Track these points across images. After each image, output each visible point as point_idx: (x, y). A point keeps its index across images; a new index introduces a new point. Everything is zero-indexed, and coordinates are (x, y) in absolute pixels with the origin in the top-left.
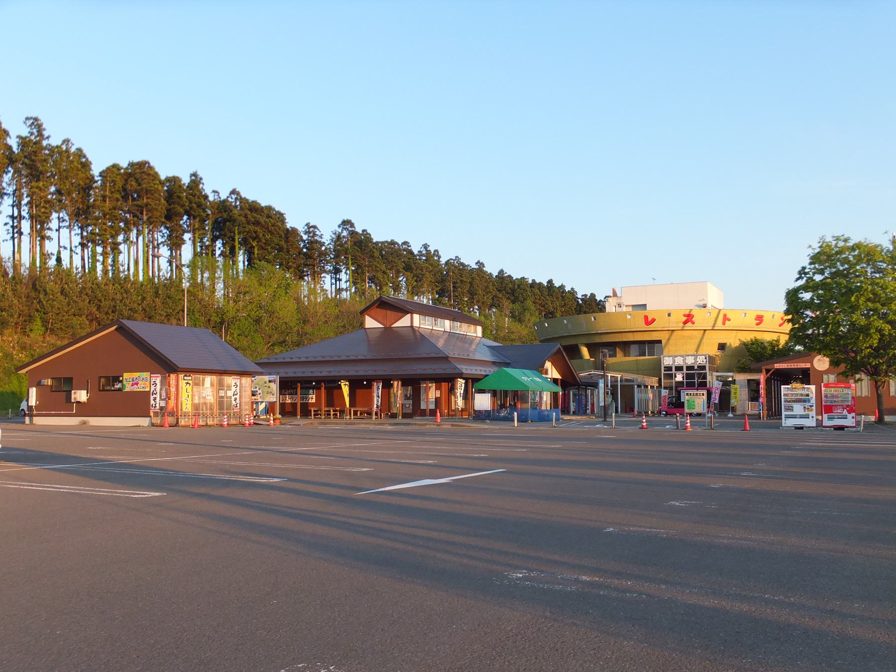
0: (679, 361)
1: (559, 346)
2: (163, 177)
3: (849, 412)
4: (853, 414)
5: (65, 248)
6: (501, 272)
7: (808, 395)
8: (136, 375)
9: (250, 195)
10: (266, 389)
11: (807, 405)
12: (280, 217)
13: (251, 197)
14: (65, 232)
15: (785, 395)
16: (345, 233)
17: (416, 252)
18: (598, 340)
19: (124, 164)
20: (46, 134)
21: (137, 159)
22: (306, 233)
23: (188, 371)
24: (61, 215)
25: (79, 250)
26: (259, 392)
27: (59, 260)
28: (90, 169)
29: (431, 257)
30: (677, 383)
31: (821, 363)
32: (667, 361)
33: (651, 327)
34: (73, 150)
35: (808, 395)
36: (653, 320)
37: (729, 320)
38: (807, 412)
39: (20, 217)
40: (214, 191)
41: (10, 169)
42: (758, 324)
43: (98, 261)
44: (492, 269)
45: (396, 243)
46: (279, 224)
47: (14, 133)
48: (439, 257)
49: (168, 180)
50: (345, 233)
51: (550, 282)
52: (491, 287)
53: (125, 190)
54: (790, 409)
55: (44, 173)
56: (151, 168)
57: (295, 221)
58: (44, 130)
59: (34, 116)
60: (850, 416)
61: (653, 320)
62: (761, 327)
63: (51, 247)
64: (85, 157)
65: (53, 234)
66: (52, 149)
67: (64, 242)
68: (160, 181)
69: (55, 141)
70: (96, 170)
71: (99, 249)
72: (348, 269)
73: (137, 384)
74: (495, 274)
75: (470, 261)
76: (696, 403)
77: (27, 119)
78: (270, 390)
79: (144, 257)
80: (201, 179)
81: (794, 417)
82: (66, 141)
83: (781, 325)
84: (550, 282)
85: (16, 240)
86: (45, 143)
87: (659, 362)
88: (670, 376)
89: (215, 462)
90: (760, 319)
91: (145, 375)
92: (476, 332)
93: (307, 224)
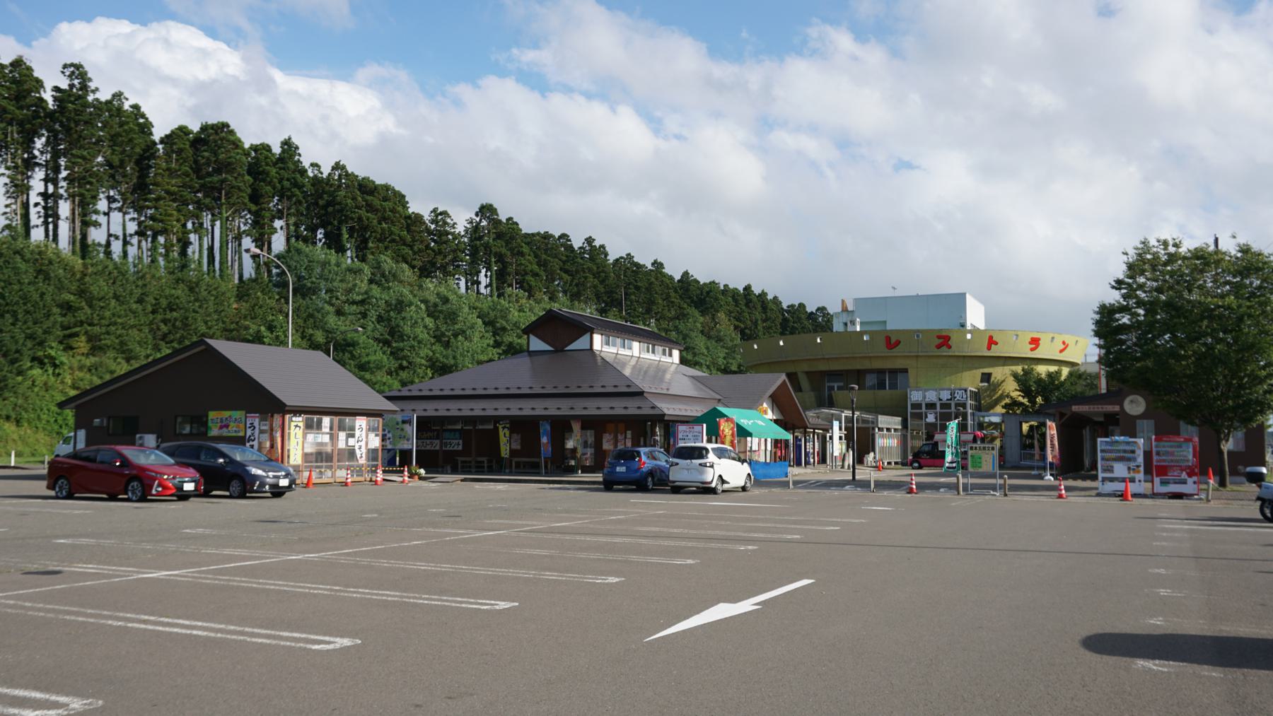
0: (931, 396)
1: (783, 377)
2: (247, 146)
3: (1190, 475)
4: (1195, 478)
5: (117, 238)
6: (686, 274)
7: (1133, 452)
8: (227, 414)
9: (359, 169)
10: (399, 432)
11: (1132, 464)
12: (400, 199)
13: (361, 173)
14: (116, 217)
15: (1102, 451)
16: (484, 223)
17: (576, 246)
18: (823, 367)
19: (195, 127)
20: (92, 85)
21: (213, 120)
22: (432, 222)
23: (297, 411)
24: (112, 193)
25: (135, 240)
27: (108, 253)
28: (151, 134)
29: (595, 252)
30: (928, 425)
31: (1135, 405)
32: (915, 396)
33: (895, 352)
34: (126, 106)
35: (1133, 452)
36: (898, 343)
37: (996, 343)
38: (1132, 474)
39: (56, 197)
40: (312, 165)
41: (44, 132)
42: (1032, 350)
43: (328, 313)
44: (674, 271)
45: (552, 236)
46: (400, 209)
47: (49, 85)
48: (606, 255)
49: (255, 148)
50: (484, 223)
51: (748, 288)
52: (673, 294)
53: (196, 162)
54: (1110, 470)
55: (85, 135)
56: (232, 132)
57: (419, 206)
58: (90, 80)
59: (76, 62)
60: (1190, 481)
61: (898, 343)
62: (1038, 354)
63: (97, 235)
64: (143, 116)
65: (102, 219)
66: (98, 105)
67: (113, 224)
68: (244, 149)
69: (104, 96)
70: (158, 133)
71: (161, 239)
72: (488, 269)
73: (227, 426)
74: (677, 277)
75: (645, 260)
77: (65, 66)
79: (231, 249)
80: (297, 148)
81: (1112, 480)
82: (118, 95)
83: (1061, 351)
84: (748, 288)
85: (51, 227)
86: (90, 98)
87: (905, 398)
88: (919, 416)
89: (385, 563)
90: (1035, 342)
91: (237, 414)
93: (435, 210)
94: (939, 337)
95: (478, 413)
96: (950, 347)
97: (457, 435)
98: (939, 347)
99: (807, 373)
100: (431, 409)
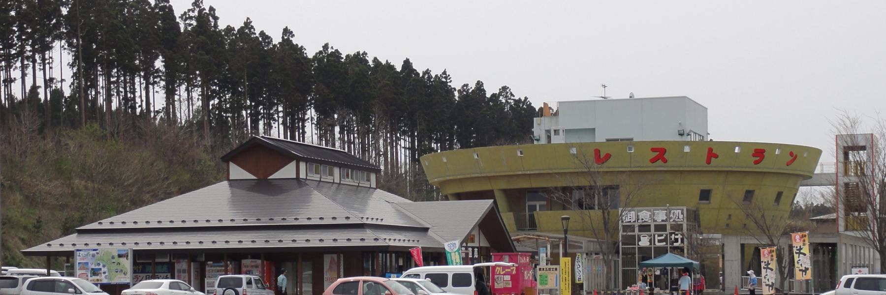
10: (115, 266)
26: (103, 270)
33: (605, 168)
36: (608, 156)
37: (716, 156)
42: (756, 162)
51: (407, 64)
61: (608, 156)
75: (346, 50)
76: (549, 278)
78: (119, 268)
88: (632, 240)
92: (369, 180)
94: (653, 150)
95: (156, 246)
96: (665, 161)
97: (165, 268)
98: (653, 161)
99: (505, 191)
100: (144, 243)
